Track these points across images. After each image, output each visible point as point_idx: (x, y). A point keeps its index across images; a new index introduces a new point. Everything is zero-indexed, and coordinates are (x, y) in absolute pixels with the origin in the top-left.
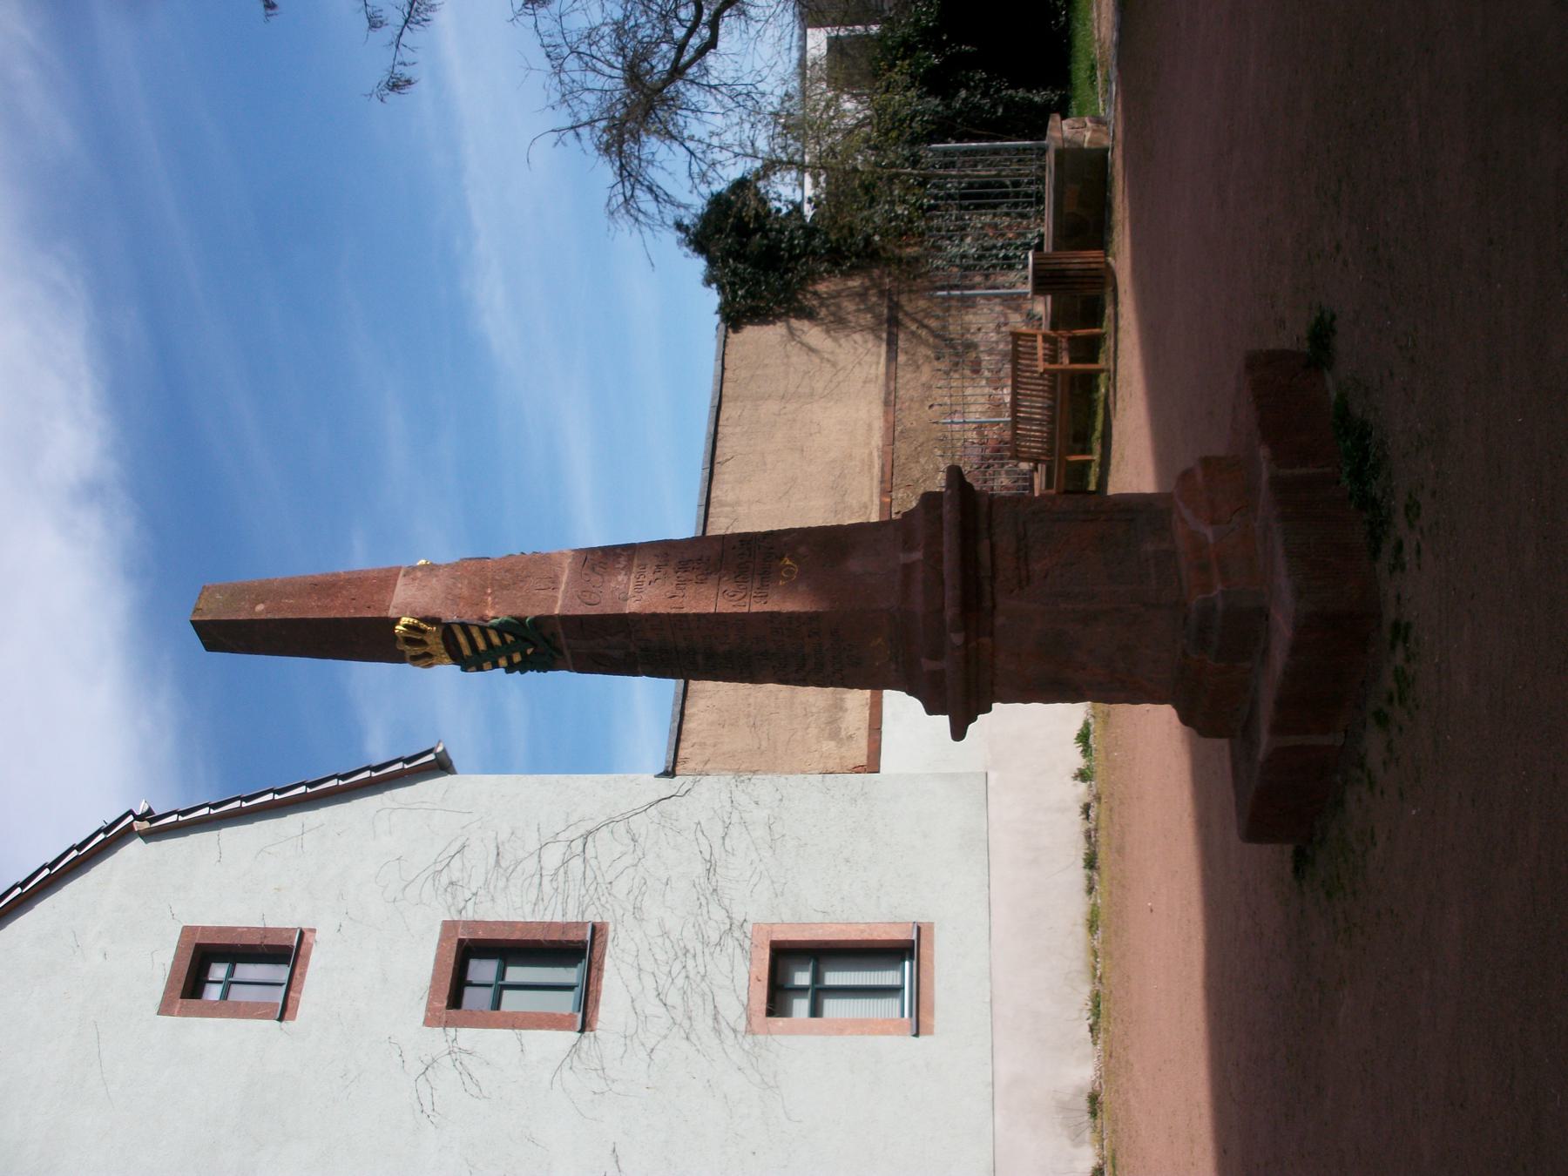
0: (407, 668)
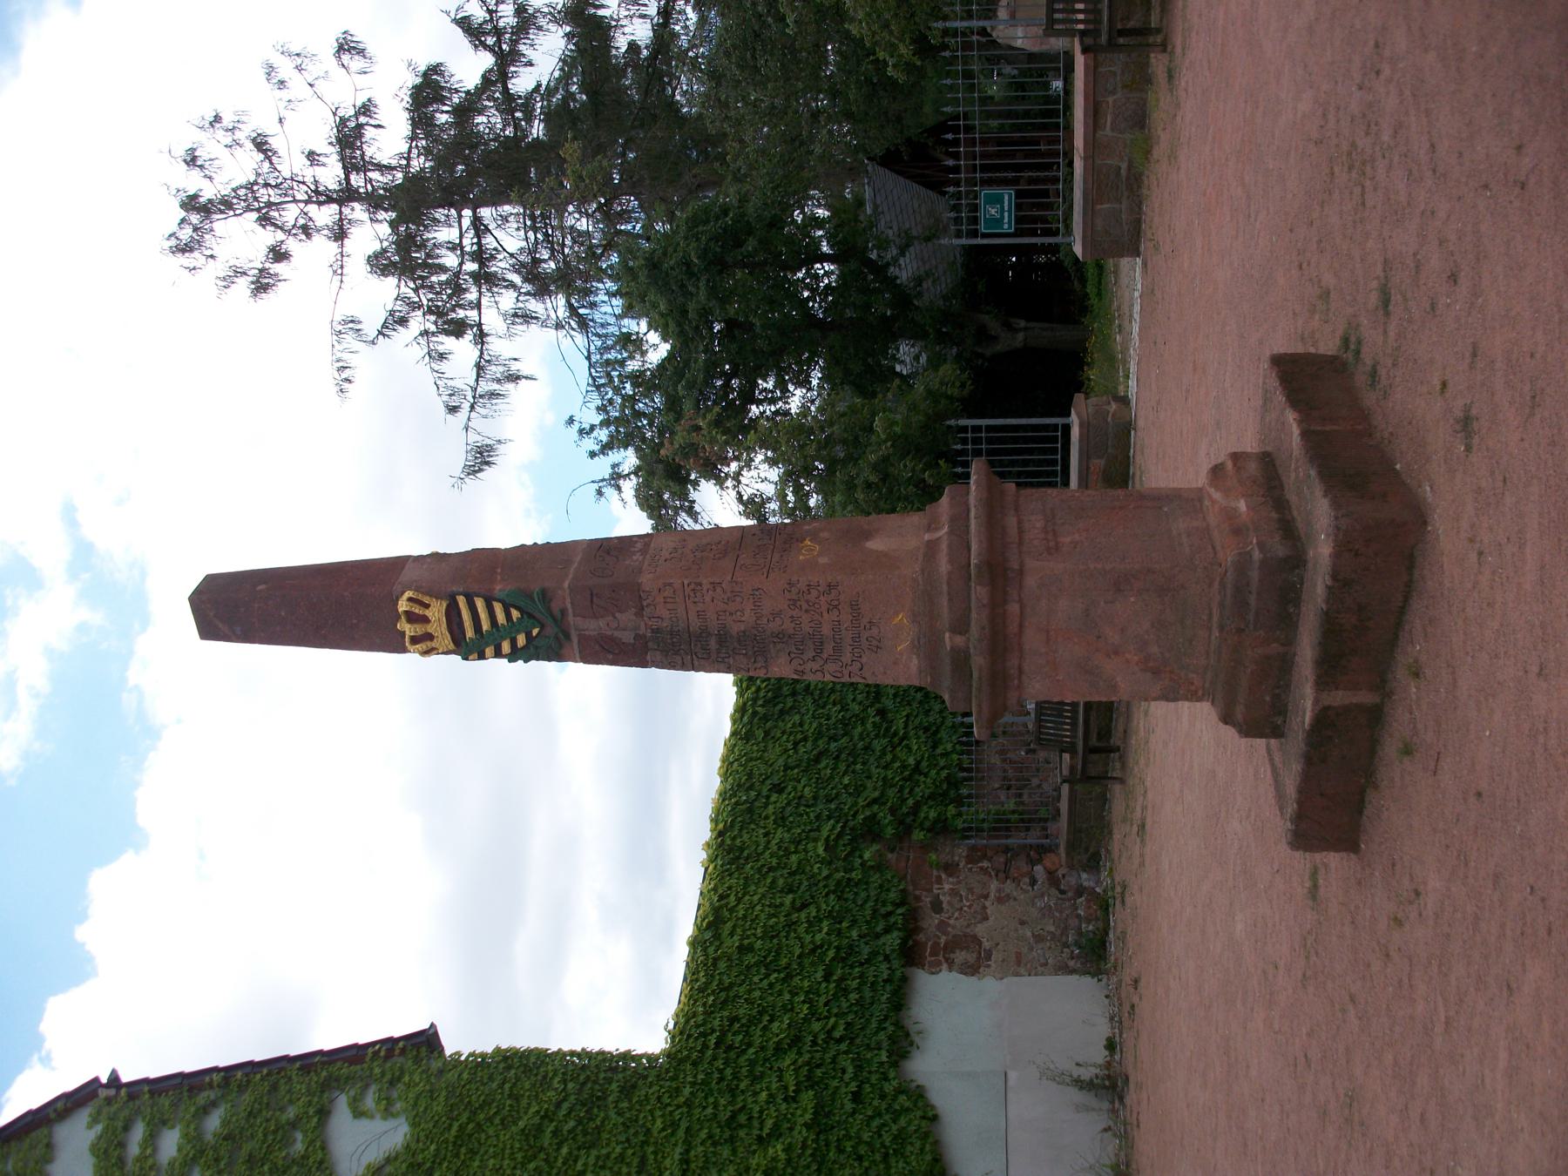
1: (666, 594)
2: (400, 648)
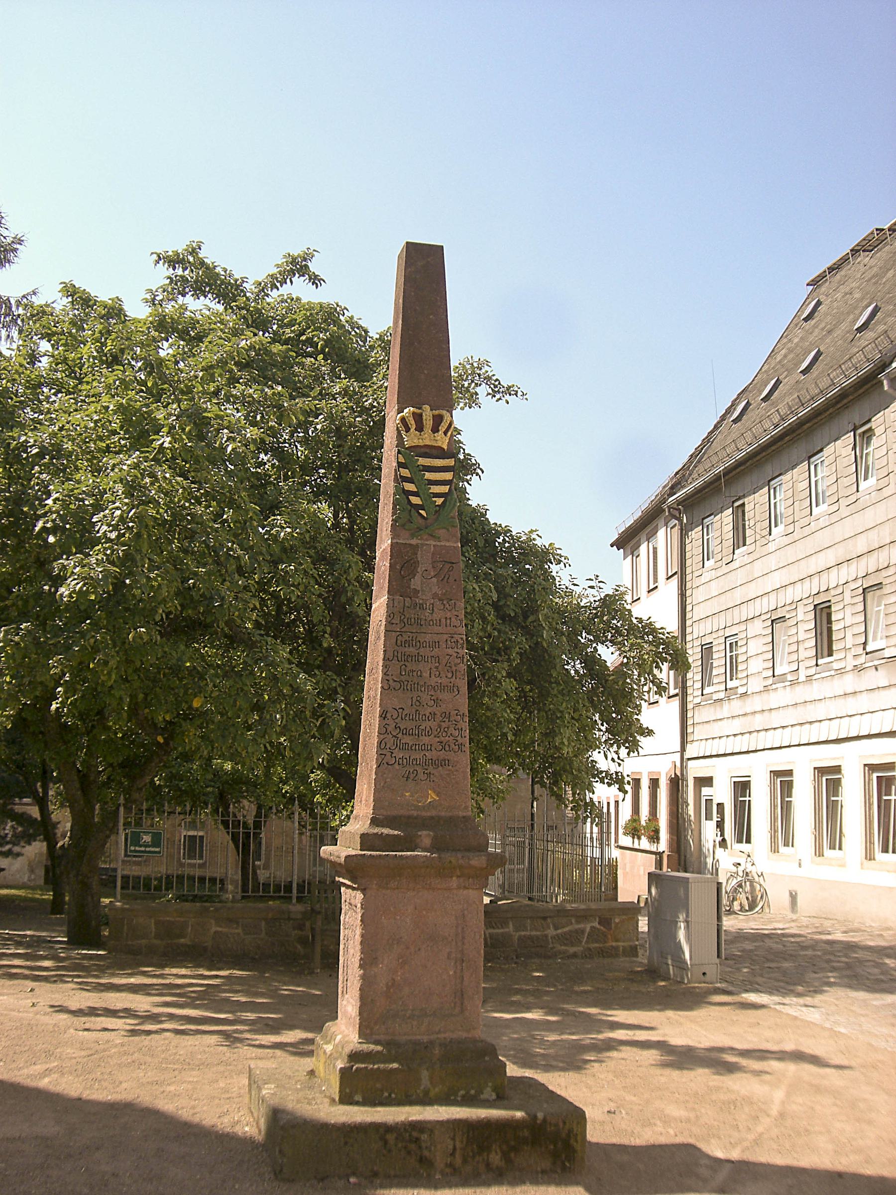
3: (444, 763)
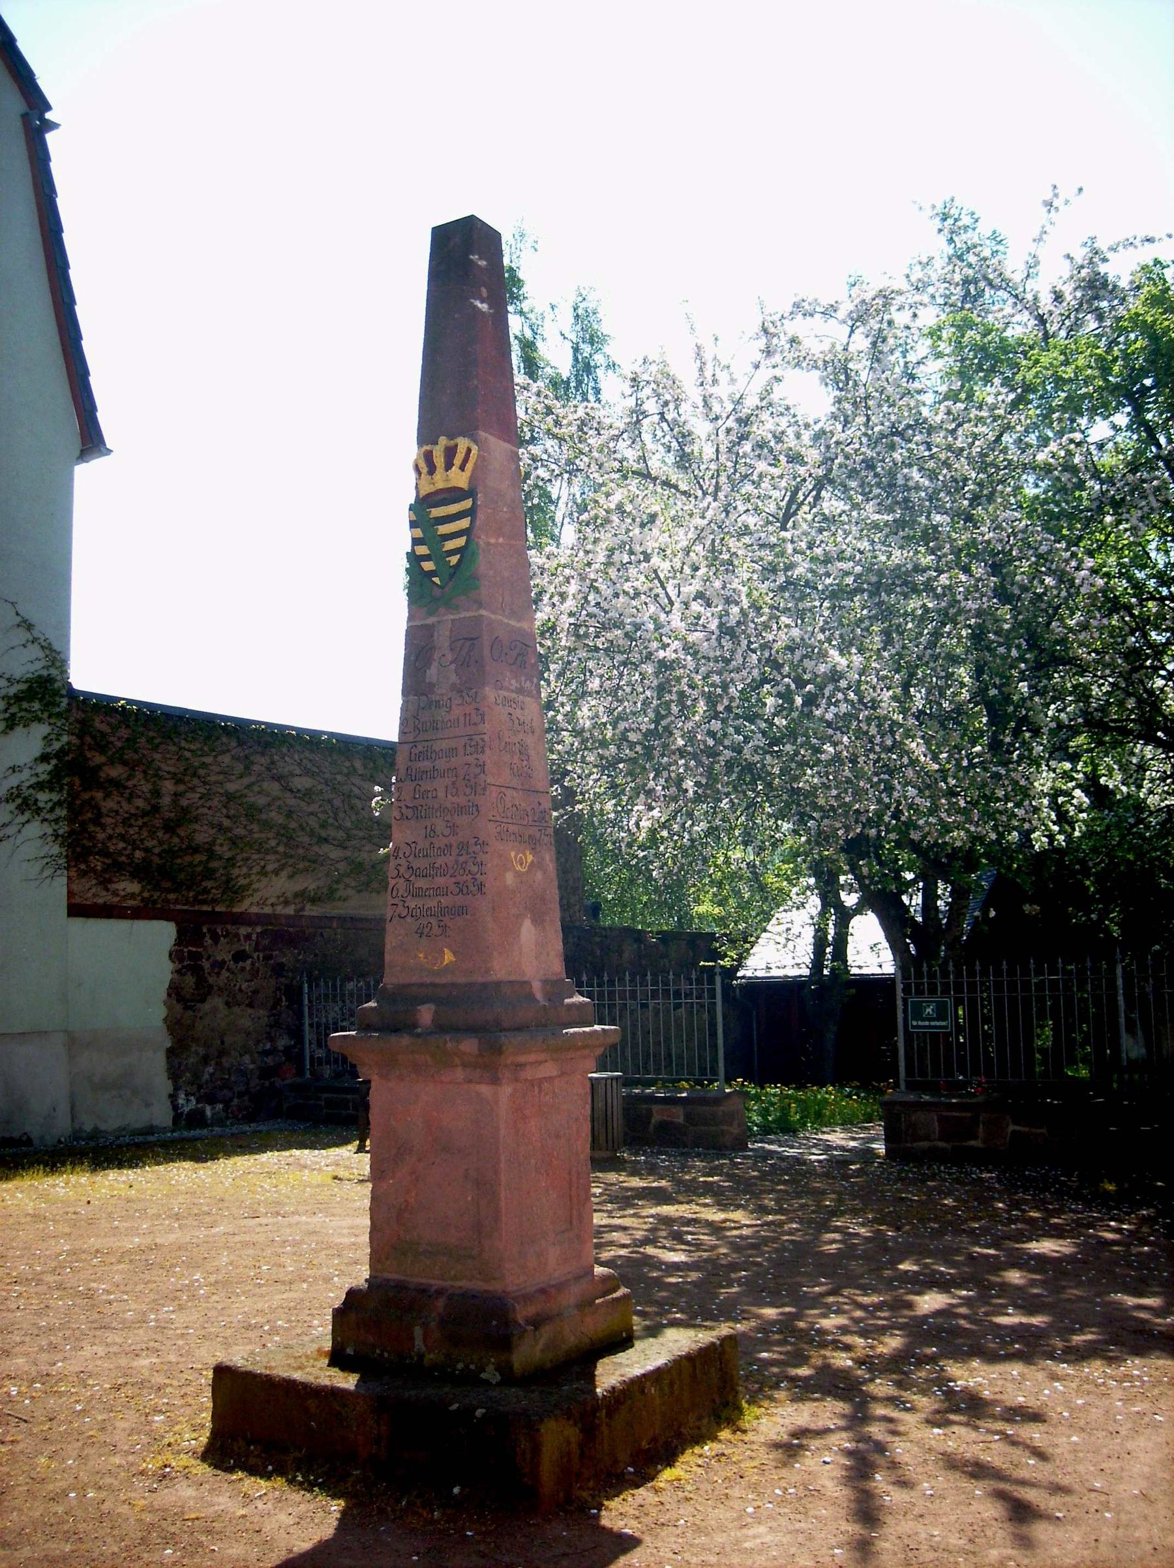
0: (412, 451)
1: (474, 715)
2: (422, 440)
3: (461, 911)
